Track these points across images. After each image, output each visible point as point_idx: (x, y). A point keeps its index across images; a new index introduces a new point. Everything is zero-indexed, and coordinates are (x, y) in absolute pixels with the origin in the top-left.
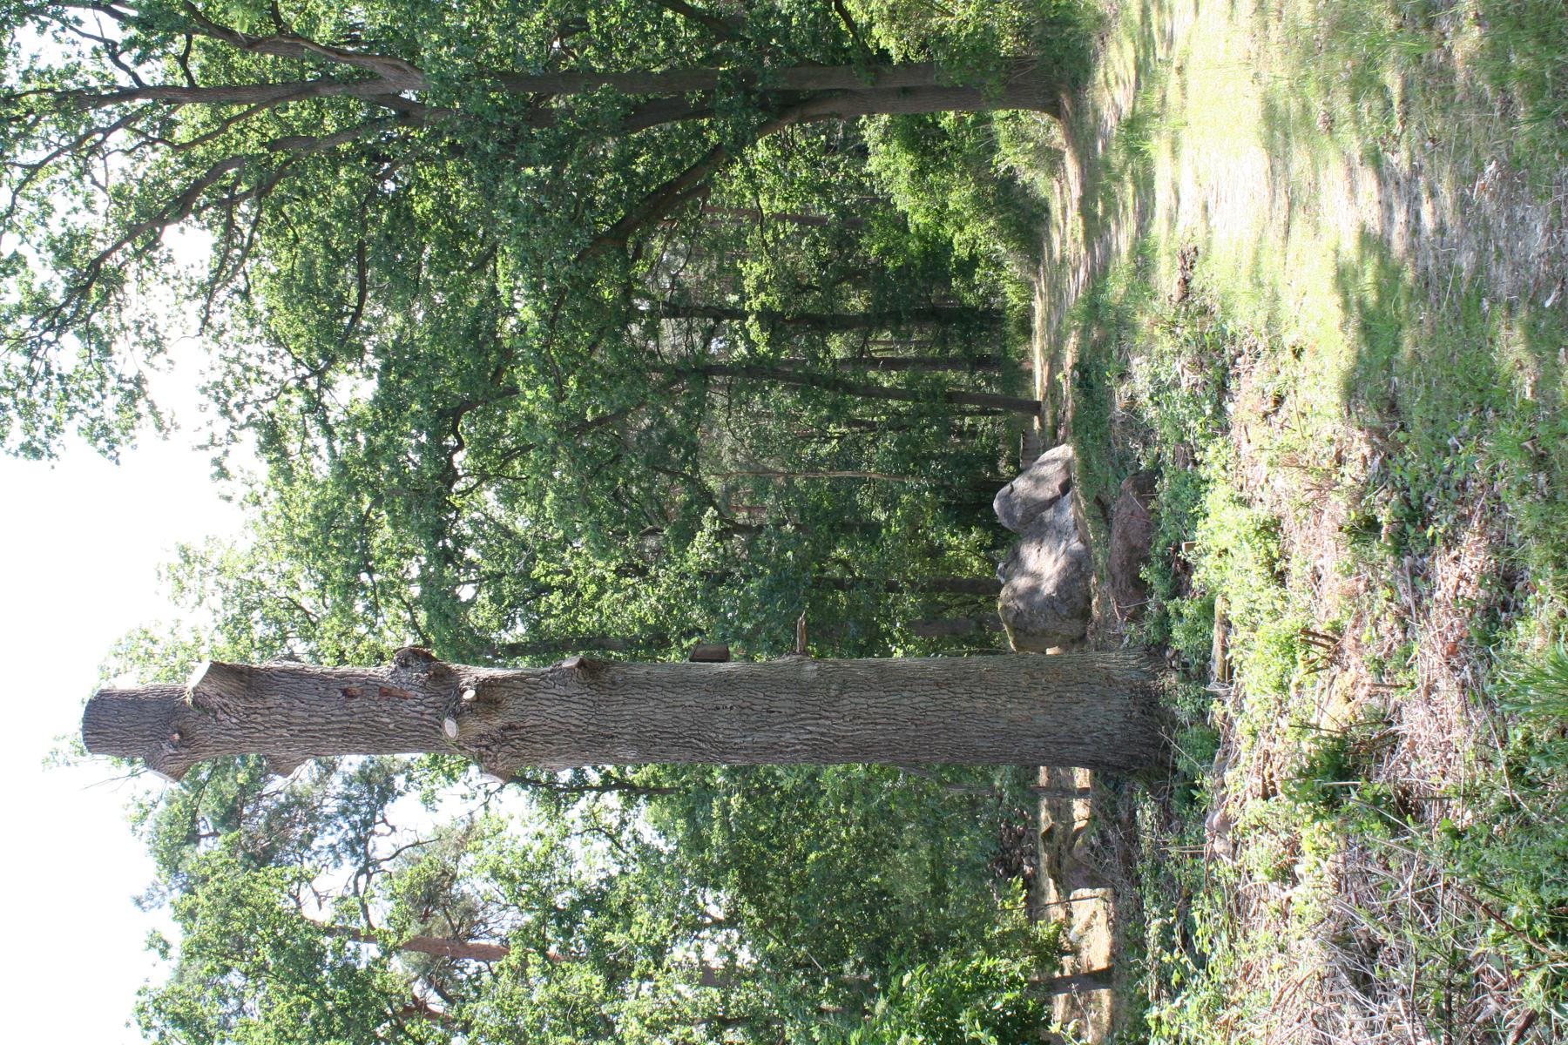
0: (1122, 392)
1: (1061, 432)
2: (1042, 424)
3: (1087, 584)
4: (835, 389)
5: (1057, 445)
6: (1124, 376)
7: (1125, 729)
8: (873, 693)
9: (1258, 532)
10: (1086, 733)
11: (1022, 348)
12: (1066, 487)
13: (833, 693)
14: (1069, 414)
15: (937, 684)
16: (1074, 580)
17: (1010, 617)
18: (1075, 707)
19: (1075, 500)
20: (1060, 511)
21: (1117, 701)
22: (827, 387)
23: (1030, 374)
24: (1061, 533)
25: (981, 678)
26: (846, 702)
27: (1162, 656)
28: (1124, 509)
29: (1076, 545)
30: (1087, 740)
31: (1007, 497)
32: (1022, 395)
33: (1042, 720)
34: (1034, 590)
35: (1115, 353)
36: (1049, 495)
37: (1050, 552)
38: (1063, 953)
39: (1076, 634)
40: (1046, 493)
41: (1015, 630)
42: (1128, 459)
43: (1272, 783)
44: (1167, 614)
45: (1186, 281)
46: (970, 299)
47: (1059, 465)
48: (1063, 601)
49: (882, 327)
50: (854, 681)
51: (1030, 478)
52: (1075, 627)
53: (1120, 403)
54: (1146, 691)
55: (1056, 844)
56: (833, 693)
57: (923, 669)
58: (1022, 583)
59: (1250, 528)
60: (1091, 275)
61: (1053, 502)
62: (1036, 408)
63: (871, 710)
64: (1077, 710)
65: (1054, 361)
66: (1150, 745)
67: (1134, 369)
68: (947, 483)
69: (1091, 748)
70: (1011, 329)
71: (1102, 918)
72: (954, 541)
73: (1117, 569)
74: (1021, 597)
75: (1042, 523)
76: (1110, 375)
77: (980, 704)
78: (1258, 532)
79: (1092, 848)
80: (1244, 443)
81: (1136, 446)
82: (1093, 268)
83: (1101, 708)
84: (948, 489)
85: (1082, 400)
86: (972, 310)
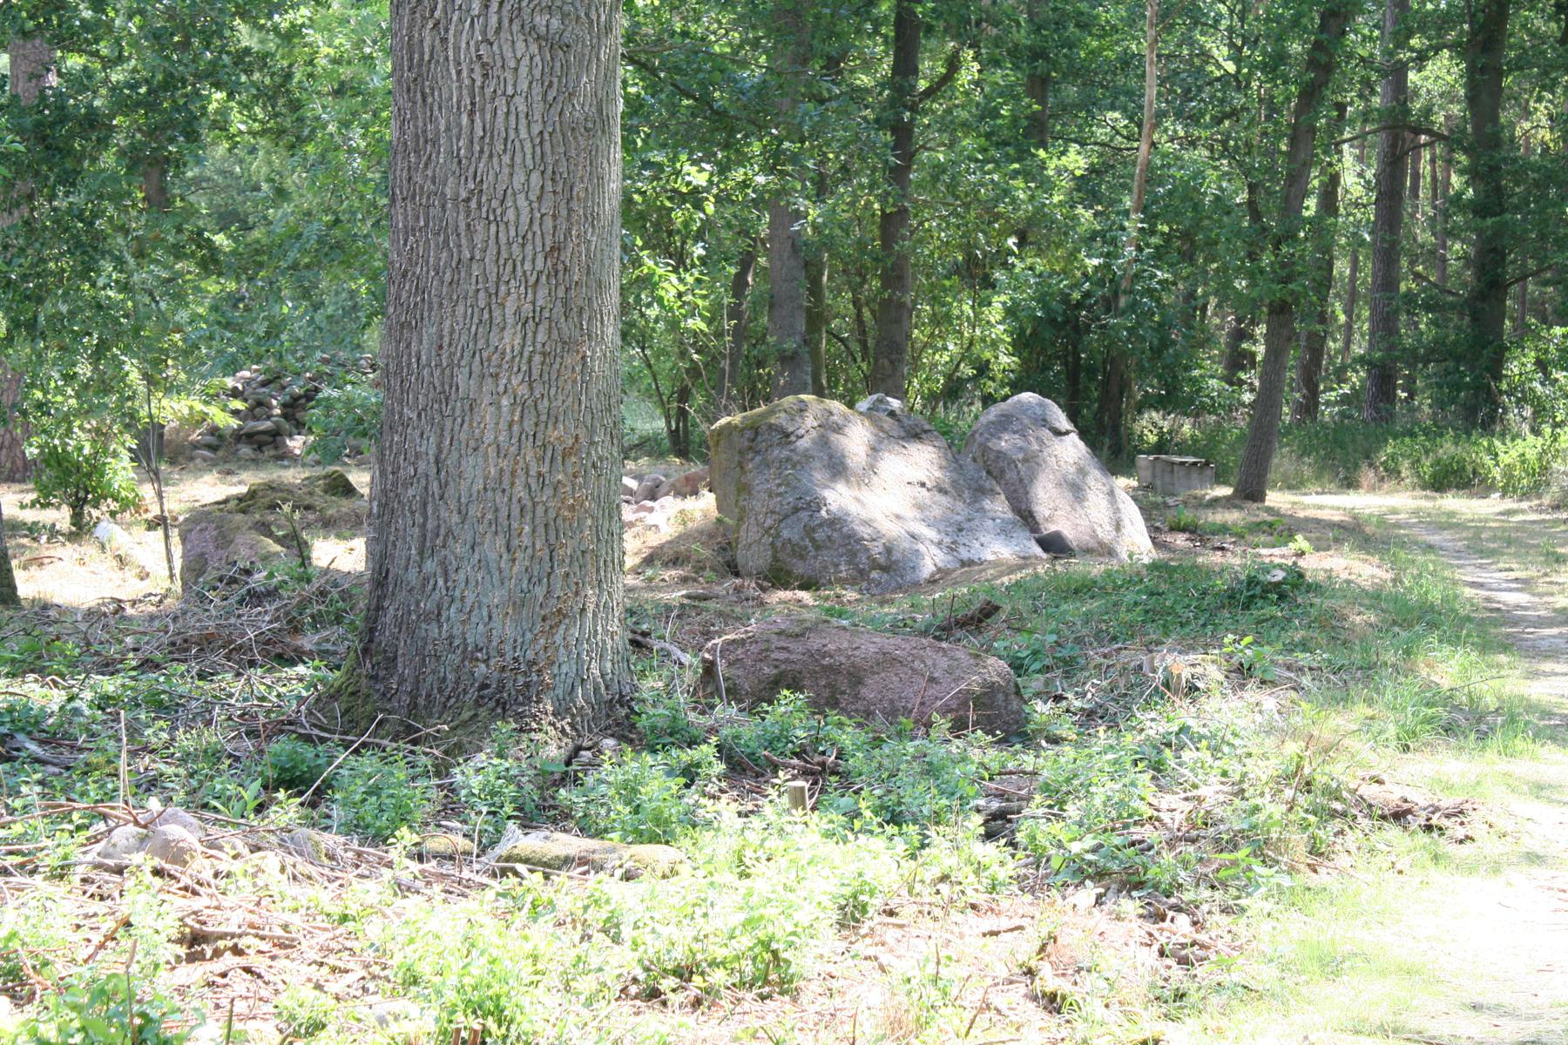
0: (1209, 668)
1: (1180, 540)
2: (1215, 503)
3: (843, 582)
4: (1312, 64)
5: (1154, 531)
6: (1242, 673)
7: (451, 648)
8: (539, 108)
9: (766, 945)
10: (443, 564)
11: (1405, 468)
12: (1054, 545)
13: (540, 20)
14: (1217, 558)
15: (557, 248)
16: (853, 555)
17: (780, 419)
18: (500, 541)
19: (1026, 561)
20: (1005, 532)
21: (510, 631)
22: (1318, 46)
23: (1350, 484)
24: (957, 531)
25: (568, 344)
26: (518, 50)
27: (605, 731)
28: (943, 663)
29: (931, 559)
30: (430, 566)
31: (1044, 422)
32: (1282, 460)
33: (474, 472)
34: (838, 468)
35: (1303, 658)
36: (1042, 510)
37: (920, 507)
38: (78, 506)
39: (741, 556)
40: (1047, 499)
41: (754, 430)
42: (1068, 675)
43: (217, 953)
44: (692, 743)
45: (1399, 816)
46: (1519, 366)
47: (1105, 533)
48: (809, 531)
49: (1474, 175)
50: (566, 67)
51: (1082, 472)
52: (754, 556)
53: (1181, 665)
54: (528, 693)
55: (318, 502)
56: (540, 20)
57: (592, 218)
58: (856, 439)
59: (780, 930)
60: (1505, 617)
61: (1026, 518)
62: (1251, 492)
63: (501, 103)
64: (493, 547)
65: (1353, 533)
66: (414, 696)
67: (1252, 694)
68: (1123, 301)
69: (413, 572)
70: (1448, 448)
71: (129, 588)
72: (995, 312)
73: (815, 642)
74: (823, 442)
75: (980, 492)
76: (1245, 649)
77: (511, 339)
78: (766, 945)
79: (248, 572)
80: (990, 923)
81: (1092, 690)
82: (1516, 622)
83: (496, 597)
84: (1109, 305)
85: (1220, 584)
86: (1495, 368)
